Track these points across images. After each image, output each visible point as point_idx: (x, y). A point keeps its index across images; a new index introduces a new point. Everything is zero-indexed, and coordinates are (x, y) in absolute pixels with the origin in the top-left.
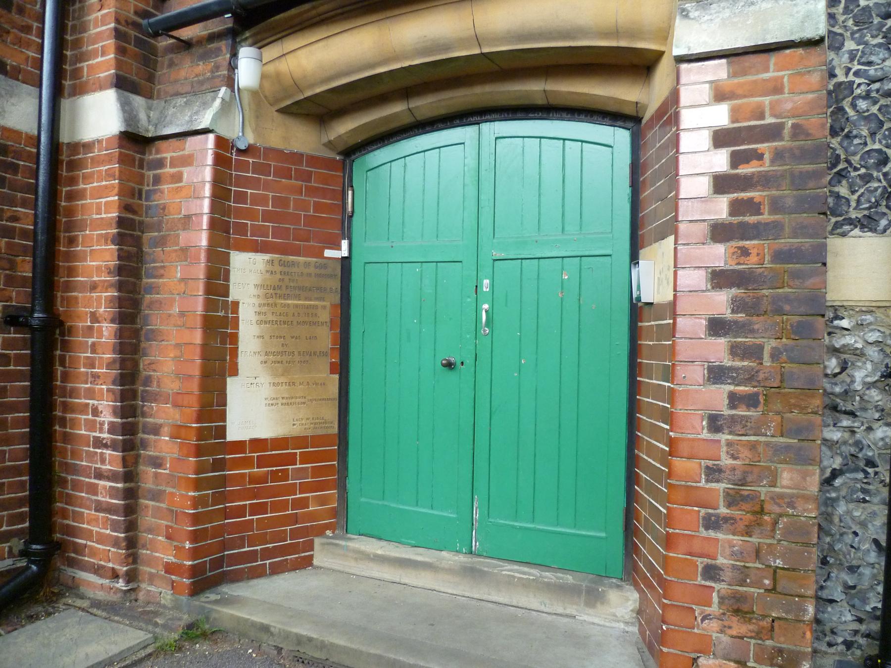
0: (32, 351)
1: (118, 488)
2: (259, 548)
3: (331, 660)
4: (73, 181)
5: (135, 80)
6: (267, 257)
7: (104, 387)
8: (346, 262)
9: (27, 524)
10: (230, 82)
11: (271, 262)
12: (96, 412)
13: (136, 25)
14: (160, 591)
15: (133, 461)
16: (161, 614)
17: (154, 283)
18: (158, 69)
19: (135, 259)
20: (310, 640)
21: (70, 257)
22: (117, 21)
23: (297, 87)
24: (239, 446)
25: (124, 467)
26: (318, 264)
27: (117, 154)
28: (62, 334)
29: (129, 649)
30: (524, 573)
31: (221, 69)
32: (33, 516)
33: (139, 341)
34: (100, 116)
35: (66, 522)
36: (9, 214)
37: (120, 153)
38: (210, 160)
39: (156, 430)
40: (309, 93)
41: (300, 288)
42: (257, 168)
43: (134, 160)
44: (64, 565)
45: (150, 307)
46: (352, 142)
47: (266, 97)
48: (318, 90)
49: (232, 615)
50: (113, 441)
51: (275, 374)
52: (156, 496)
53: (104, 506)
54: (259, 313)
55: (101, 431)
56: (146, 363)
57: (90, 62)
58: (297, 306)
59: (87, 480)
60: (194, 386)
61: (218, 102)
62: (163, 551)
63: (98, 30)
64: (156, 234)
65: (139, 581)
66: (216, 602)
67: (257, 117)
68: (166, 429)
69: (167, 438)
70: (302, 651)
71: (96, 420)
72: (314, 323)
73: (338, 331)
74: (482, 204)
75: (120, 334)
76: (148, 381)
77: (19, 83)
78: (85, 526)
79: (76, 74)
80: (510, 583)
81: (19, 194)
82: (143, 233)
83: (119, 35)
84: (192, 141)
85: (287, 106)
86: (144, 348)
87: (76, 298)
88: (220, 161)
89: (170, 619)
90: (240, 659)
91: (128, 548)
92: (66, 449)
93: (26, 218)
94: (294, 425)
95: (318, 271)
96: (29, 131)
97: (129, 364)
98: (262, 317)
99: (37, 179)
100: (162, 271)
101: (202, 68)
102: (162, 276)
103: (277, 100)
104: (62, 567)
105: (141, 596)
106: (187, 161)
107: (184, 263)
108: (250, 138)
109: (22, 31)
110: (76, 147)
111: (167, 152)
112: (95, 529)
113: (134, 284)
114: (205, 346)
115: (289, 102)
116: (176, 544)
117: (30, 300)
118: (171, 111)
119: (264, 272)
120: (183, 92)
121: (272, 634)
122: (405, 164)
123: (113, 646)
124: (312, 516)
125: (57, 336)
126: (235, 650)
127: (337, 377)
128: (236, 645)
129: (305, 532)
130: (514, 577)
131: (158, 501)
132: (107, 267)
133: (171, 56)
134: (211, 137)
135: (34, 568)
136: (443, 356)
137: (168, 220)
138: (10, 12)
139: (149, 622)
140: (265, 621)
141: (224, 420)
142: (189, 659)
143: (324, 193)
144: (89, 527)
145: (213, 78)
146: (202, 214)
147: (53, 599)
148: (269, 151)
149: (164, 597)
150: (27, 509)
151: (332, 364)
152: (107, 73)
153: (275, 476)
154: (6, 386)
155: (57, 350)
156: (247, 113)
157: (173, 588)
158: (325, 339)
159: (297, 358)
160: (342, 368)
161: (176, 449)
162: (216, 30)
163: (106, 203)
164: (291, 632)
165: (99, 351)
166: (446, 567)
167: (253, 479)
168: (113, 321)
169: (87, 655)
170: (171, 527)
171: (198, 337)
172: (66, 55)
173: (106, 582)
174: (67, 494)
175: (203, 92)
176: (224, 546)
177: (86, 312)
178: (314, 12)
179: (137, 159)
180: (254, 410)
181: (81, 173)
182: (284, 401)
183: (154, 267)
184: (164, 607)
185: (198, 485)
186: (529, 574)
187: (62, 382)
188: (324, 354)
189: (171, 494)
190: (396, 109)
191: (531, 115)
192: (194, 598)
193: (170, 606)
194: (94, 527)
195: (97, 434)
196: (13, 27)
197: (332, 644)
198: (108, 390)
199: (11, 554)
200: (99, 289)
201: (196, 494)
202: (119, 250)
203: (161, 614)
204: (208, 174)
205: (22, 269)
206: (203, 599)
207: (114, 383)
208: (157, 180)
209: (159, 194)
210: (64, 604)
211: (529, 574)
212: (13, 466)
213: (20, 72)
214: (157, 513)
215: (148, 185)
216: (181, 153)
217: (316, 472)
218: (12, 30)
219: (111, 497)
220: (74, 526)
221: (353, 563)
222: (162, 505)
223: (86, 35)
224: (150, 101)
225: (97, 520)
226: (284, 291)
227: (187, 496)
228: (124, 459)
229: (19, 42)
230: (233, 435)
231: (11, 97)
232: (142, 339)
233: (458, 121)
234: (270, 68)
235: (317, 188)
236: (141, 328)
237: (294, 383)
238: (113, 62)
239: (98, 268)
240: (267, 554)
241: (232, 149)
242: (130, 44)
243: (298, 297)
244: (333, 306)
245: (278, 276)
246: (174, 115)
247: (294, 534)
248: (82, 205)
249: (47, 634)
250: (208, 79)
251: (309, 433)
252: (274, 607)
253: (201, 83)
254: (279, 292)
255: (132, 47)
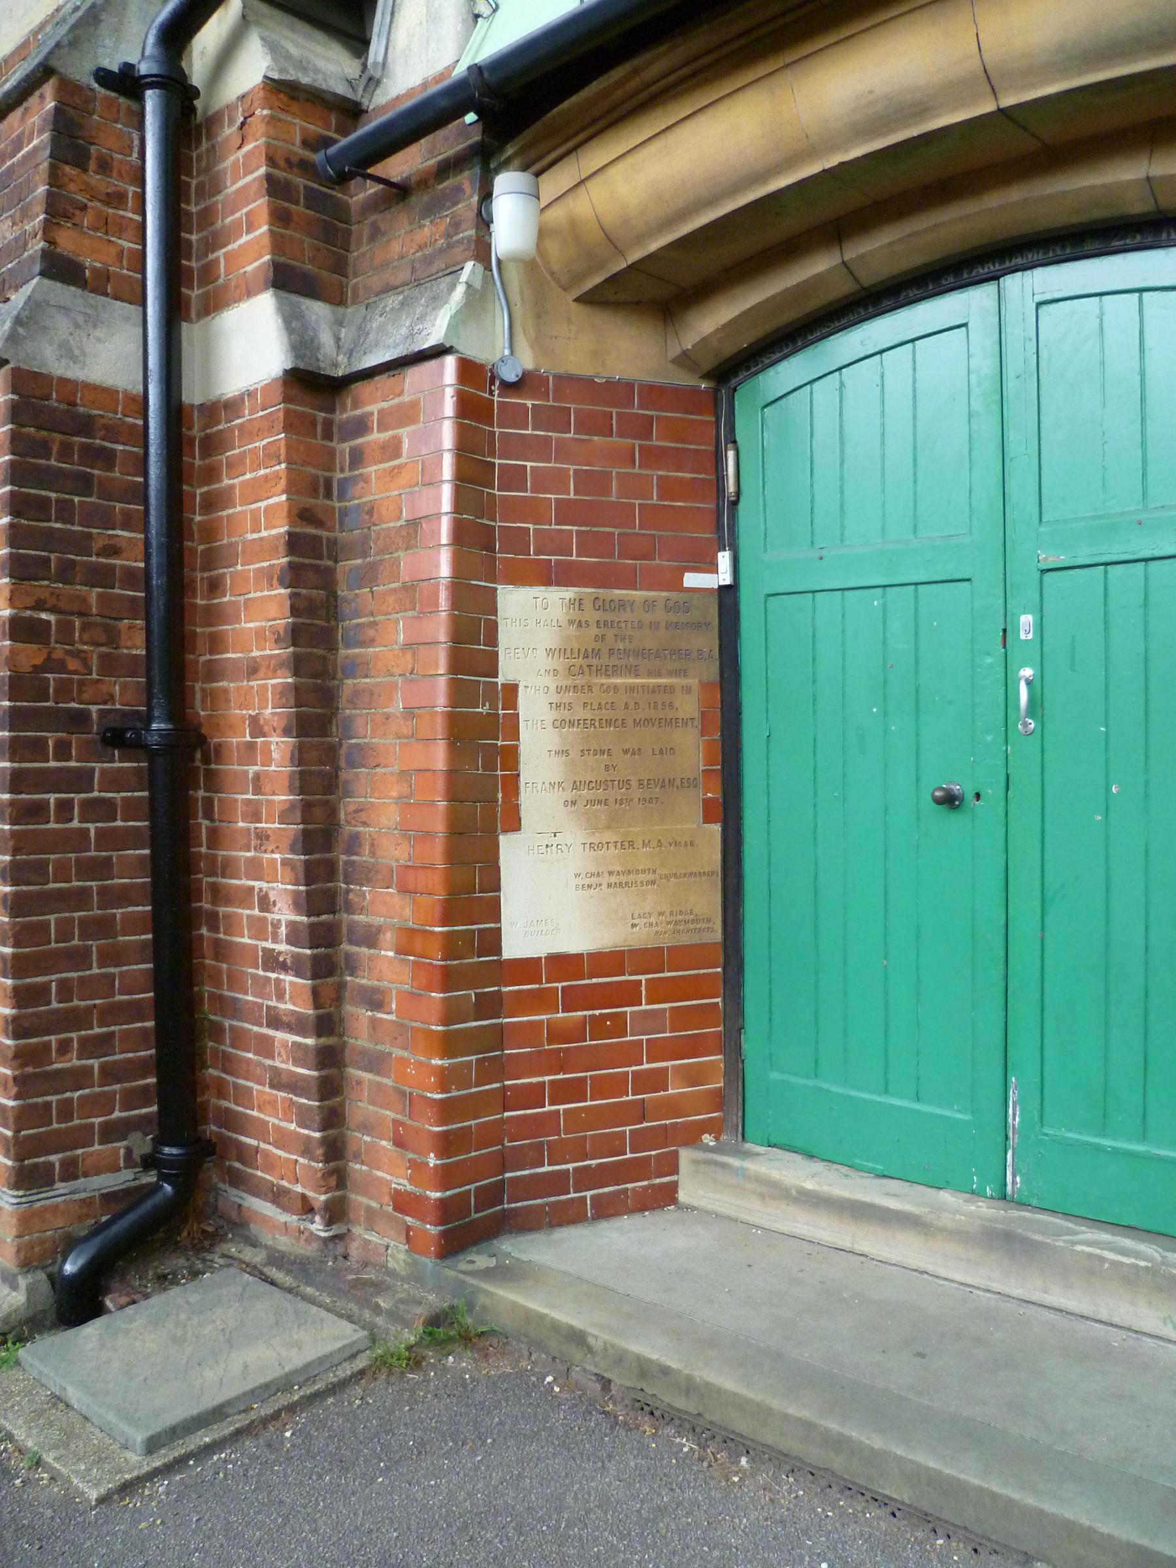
0: (151, 791)
1: (307, 1046)
2: (570, 1166)
3: (707, 1417)
4: (211, 474)
5: (310, 273)
6: (570, 593)
7: (277, 856)
8: (728, 596)
9: (155, 1108)
10: (482, 250)
11: (579, 603)
12: (265, 904)
13: (305, 166)
14: (387, 1245)
15: (334, 996)
16: (388, 1288)
17: (357, 656)
18: (353, 246)
19: (323, 612)
20: (666, 1371)
21: (213, 615)
22: (271, 161)
23: (614, 246)
24: (527, 968)
25: (317, 1006)
26: (671, 604)
27: (281, 414)
28: (206, 760)
29: (322, 1360)
30: (1125, 1252)
31: (463, 226)
32: (163, 1094)
33: (337, 769)
34: (249, 345)
35: (225, 1104)
36: (101, 543)
37: (287, 412)
38: (449, 407)
39: (371, 938)
40: (636, 255)
41: (637, 653)
42: (546, 419)
43: (314, 424)
44: (224, 1182)
45: (352, 703)
46: (730, 348)
47: (552, 274)
48: (654, 246)
49: (515, 1304)
50: (296, 956)
51: (593, 828)
52: (375, 1063)
53: (284, 1078)
54: (558, 706)
55: (275, 941)
56: (351, 808)
57: (230, 247)
58: (632, 689)
59: (256, 1029)
60: (436, 854)
61: (459, 291)
62: (389, 1169)
63: (240, 184)
64: (359, 561)
65: (349, 1221)
66: (487, 1274)
67: (539, 316)
68: (388, 937)
69: (391, 954)
70: (649, 1390)
71: (266, 919)
72: (669, 723)
73: (717, 736)
74: (1012, 449)
75: (300, 756)
76: (354, 842)
77: (109, 300)
78: (255, 1113)
79: (208, 273)
80: (1091, 1271)
81: (118, 505)
82: (336, 561)
83: (275, 187)
84: (415, 376)
85: (596, 288)
86: (346, 782)
87: (226, 691)
88: (471, 409)
89: (401, 1301)
90: (529, 1394)
91: (327, 1159)
92: (219, 971)
93: (133, 547)
94: (634, 926)
95: (672, 617)
96: (129, 387)
97: (318, 812)
98: (565, 714)
99: (146, 474)
100: (371, 633)
101: (430, 231)
102: (371, 642)
103: (577, 278)
104: (221, 1185)
105: (354, 1249)
106: (406, 415)
107: (411, 614)
108: (526, 360)
109: (108, 204)
110: (216, 410)
111: (373, 402)
112: (272, 1120)
113: (324, 659)
114: (452, 774)
115: (598, 279)
116: (411, 1156)
117: (144, 698)
118: (376, 322)
119: (565, 624)
120: (397, 283)
121: (590, 1350)
122: (842, 384)
123: (294, 1352)
124: (673, 1107)
125: (198, 763)
126: (521, 1374)
127: (717, 828)
128: (524, 1364)
129: (662, 1137)
130: (1102, 1259)
131: (378, 1073)
132: (274, 630)
133: (373, 218)
134: (450, 361)
135: (168, 1188)
136: (935, 781)
137: (378, 533)
138: (85, 170)
139: (365, 1302)
140: (578, 1323)
141: (498, 919)
142: (432, 1387)
143: (677, 458)
144: (262, 1116)
145: (450, 246)
146: (438, 516)
147: (205, 1243)
148: (566, 382)
149: (393, 1256)
150: (153, 1080)
151: (706, 802)
152: (257, 264)
153: (598, 1027)
154: (111, 857)
155: (197, 788)
156: (518, 310)
157: (408, 1240)
158: (692, 752)
159: (637, 793)
160: (728, 811)
161: (407, 974)
162: (450, 153)
163: (267, 509)
164: (626, 1351)
165: (267, 788)
166: (951, 1225)
167: (557, 1033)
168: (286, 732)
169: (246, 1366)
170: (402, 1124)
171: (439, 757)
172: (189, 242)
173: (292, 1219)
174: (224, 1052)
175: (434, 278)
176: (503, 1162)
177: (243, 716)
178: (634, 83)
179: (320, 421)
180: (557, 895)
181: (223, 458)
182: (613, 879)
183: (358, 625)
184: (393, 1274)
185: (449, 1045)
186: (1137, 1255)
187: (209, 848)
188: (690, 783)
189: (403, 1061)
190: (819, 266)
191: (1116, 243)
192: (447, 1262)
193: (403, 1273)
194: (270, 1115)
195: (269, 945)
196: (93, 198)
197: (709, 1386)
198: (284, 862)
199: (129, 1162)
200: (261, 673)
201: (446, 1062)
202: (292, 596)
203: (388, 1288)
204: (447, 435)
205: (129, 643)
206: (463, 1266)
207: (293, 850)
208: (357, 458)
209: (362, 484)
210: (224, 1256)
211: (1137, 1255)
212: (129, 1003)
213: (108, 280)
214: (379, 1095)
215: (342, 470)
216: (397, 401)
217: (681, 1018)
218: (89, 204)
219: (295, 1064)
220: (238, 1112)
221: (756, 1205)
222: (385, 1081)
223: (219, 198)
224: (340, 310)
225: (273, 1103)
226: (605, 660)
227: (429, 1065)
228: (315, 993)
229: (104, 224)
230: (514, 947)
231: (95, 326)
232: (342, 763)
233: (951, 279)
234: (557, 214)
235: (663, 451)
236: (341, 745)
237: (631, 844)
238: (266, 241)
239: (259, 633)
240: (586, 1179)
241: (492, 383)
242: (297, 203)
243: (635, 671)
244: (704, 685)
245: (594, 630)
246: (381, 329)
247: (640, 1140)
248: (228, 516)
249: (183, 1317)
250: (441, 250)
251: (665, 942)
252: (597, 1293)
253: (429, 260)
254: (595, 662)
255: (301, 208)
